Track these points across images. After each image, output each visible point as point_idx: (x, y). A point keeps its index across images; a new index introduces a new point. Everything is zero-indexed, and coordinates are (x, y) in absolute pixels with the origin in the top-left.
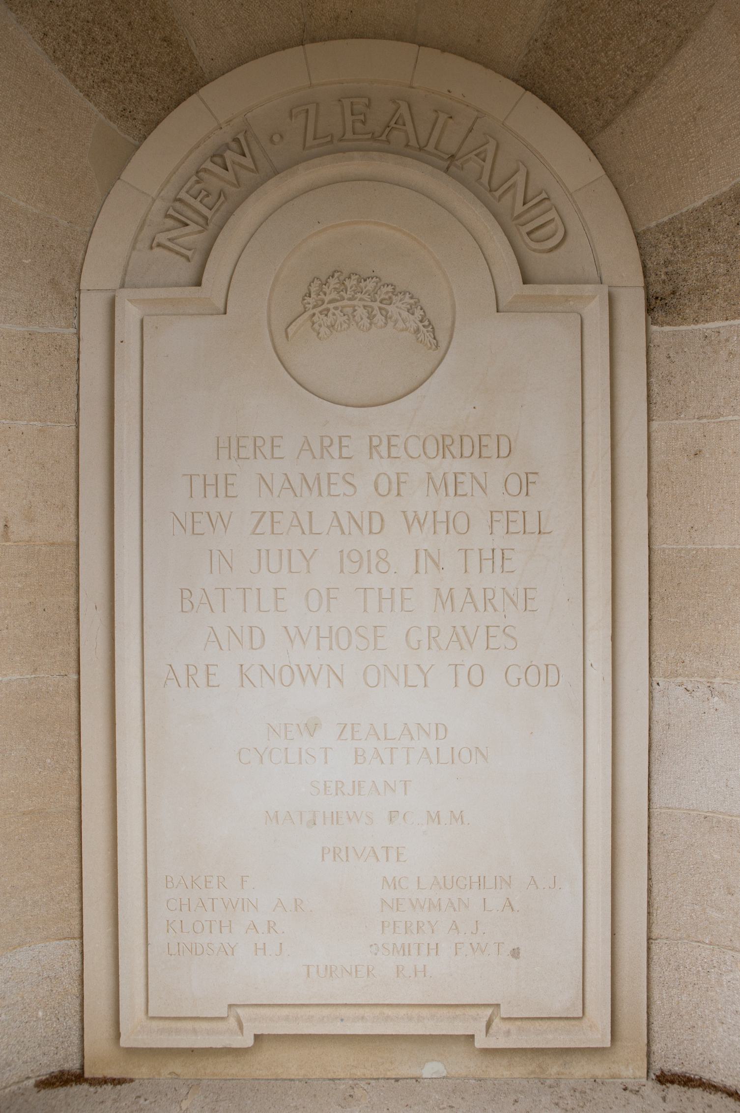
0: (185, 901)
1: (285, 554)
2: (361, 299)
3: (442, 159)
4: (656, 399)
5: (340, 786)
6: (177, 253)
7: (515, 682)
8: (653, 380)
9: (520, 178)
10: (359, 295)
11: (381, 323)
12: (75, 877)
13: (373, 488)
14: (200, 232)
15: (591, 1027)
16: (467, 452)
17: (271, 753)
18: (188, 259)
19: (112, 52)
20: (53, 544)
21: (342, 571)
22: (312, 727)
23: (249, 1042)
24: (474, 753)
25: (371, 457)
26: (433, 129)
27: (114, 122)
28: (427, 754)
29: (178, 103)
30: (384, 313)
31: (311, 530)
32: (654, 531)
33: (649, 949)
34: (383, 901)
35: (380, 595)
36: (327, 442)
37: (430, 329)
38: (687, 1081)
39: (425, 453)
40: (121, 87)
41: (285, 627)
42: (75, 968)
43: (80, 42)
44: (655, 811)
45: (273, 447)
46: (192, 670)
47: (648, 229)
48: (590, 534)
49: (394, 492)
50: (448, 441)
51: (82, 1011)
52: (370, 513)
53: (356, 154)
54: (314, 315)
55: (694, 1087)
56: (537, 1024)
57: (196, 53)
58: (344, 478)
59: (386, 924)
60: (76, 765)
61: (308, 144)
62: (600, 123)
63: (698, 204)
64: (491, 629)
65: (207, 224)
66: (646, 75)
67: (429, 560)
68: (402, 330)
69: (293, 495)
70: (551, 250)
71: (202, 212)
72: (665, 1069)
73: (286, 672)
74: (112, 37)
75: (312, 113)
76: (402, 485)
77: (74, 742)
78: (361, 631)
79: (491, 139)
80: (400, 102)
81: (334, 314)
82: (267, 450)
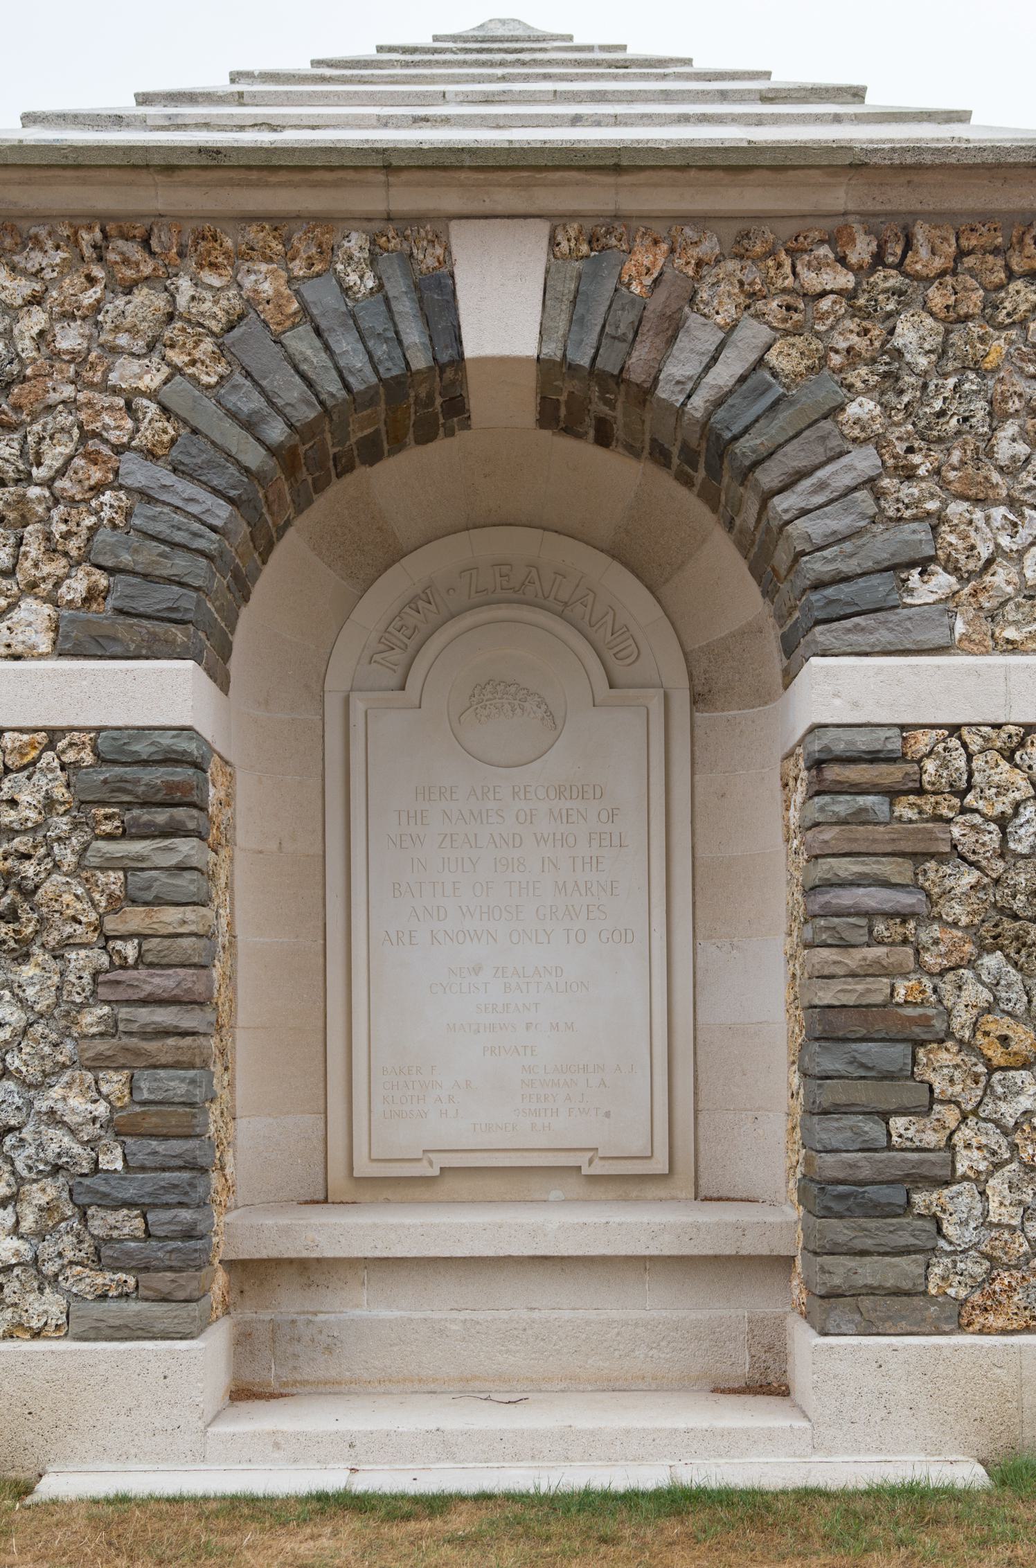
9: (609, 618)
12: (322, 1073)
22: (477, 970)
23: (437, 1173)
36: (486, 790)
44: (699, 1027)
71: (406, 642)
73: (461, 935)
77: (321, 984)
82: (448, 795)
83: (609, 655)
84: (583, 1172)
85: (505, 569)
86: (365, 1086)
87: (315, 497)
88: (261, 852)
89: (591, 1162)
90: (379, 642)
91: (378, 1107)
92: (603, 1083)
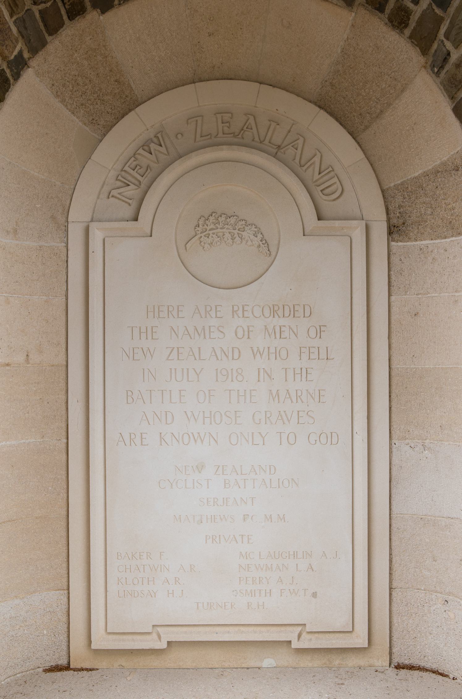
0: (128, 567)
1: (185, 371)
2: (227, 229)
3: (273, 148)
4: (394, 283)
5: (216, 500)
6: (123, 201)
7: (314, 442)
8: (392, 273)
9: (317, 159)
10: (226, 226)
11: (239, 242)
12: (65, 555)
13: (234, 334)
14: (136, 189)
15: (357, 637)
16: (287, 313)
17: (177, 482)
18: (130, 205)
19: (87, 89)
20: (53, 366)
21: (217, 380)
22: (200, 468)
23: (165, 646)
24: (291, 482)
25: (233, 317)
26: (268, 131)
27: (87, 127)
28: (265, 482)
29: (123, 117)
30: (240, 236)
31: (200, 357)
32: (392, 358)
33: (390, 594)
34: (240, 566)
35: (238, 393)
36: (208, 309)
37: (266, 245)
38: (411, 668)
39: (263, 315)
40: (91, 107)
41: (185, 412)
42: (65, 607)
43: (71, 86)
45: (178, 311)
46: (133, 436)
47: (390, 188)
48: (355, 360)
49: (246, 336)
50: (276, 308)
51: (69, 632)
52: (233, 348)
53: (224, 147)
54: (201, 237)
55: (415, 670)
56: (327, 635)
57: (134, 87)
58: (218, 329)
59: (242, 579)
60: (65, 491)
61: (197, 140)
62: (363, 127)
63: (416, 174)
64: (300, 413)
65: (140, 184)
66: (387, 103)
67: (265, 374)
68: (251, 246)
69: (189, 338)
70: (334, 200)
71: (139, 178)
72: (400, 662)
73: (186, 437)
74: (87, 82)
75: (199, 122)
76: (250, 333)
77: (64, 478)
78: (228, 414)
79: (300, 137)
80: (250, 116)
81: (212, 237)
83: (317, 192)
84: (293, 646)
85: (227, 117)
86: (102, 568)
87: (49, 38)
88: (8, 365)
89: (299, 636)
90: (117, 180)
91: (113, 587)
92: (311, 567)
